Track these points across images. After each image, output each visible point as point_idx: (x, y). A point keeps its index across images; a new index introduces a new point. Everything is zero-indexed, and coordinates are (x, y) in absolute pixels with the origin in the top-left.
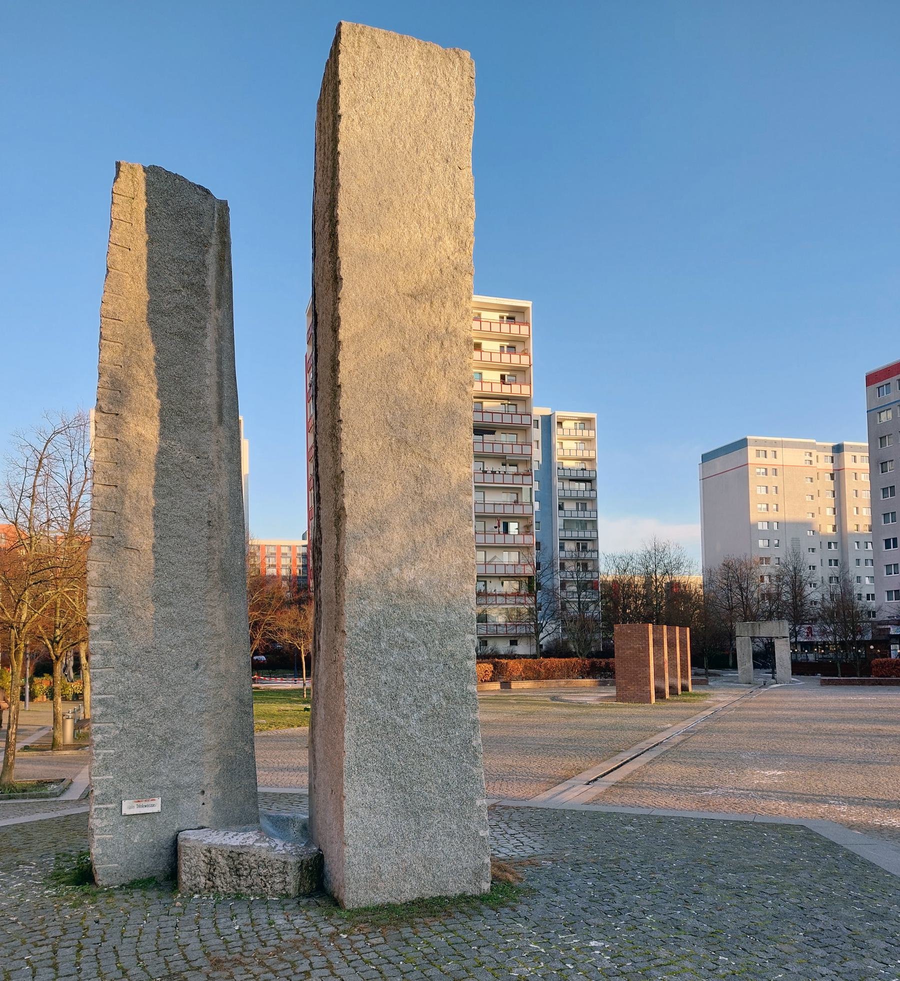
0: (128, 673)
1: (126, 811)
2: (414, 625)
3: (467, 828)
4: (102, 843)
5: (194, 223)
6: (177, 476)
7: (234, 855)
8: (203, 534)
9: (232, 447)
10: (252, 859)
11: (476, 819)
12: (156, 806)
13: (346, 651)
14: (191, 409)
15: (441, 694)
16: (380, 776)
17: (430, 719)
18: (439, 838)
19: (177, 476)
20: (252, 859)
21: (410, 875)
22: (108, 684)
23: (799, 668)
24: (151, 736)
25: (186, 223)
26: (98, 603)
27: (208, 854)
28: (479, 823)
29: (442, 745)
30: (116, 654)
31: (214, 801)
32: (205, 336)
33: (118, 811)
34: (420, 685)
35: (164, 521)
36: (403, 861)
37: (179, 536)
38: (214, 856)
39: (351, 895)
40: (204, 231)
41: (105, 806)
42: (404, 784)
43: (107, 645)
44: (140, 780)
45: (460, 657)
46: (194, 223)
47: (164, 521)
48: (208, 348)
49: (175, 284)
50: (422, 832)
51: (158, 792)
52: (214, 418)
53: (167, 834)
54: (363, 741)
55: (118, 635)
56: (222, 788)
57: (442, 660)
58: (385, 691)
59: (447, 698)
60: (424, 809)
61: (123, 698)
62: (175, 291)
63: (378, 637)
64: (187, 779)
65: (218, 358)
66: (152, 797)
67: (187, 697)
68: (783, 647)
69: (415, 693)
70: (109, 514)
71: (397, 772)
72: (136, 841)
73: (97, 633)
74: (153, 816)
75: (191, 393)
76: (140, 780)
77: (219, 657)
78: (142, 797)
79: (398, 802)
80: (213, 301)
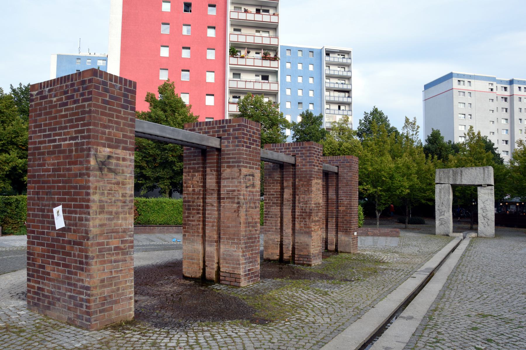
68: (486, 197)
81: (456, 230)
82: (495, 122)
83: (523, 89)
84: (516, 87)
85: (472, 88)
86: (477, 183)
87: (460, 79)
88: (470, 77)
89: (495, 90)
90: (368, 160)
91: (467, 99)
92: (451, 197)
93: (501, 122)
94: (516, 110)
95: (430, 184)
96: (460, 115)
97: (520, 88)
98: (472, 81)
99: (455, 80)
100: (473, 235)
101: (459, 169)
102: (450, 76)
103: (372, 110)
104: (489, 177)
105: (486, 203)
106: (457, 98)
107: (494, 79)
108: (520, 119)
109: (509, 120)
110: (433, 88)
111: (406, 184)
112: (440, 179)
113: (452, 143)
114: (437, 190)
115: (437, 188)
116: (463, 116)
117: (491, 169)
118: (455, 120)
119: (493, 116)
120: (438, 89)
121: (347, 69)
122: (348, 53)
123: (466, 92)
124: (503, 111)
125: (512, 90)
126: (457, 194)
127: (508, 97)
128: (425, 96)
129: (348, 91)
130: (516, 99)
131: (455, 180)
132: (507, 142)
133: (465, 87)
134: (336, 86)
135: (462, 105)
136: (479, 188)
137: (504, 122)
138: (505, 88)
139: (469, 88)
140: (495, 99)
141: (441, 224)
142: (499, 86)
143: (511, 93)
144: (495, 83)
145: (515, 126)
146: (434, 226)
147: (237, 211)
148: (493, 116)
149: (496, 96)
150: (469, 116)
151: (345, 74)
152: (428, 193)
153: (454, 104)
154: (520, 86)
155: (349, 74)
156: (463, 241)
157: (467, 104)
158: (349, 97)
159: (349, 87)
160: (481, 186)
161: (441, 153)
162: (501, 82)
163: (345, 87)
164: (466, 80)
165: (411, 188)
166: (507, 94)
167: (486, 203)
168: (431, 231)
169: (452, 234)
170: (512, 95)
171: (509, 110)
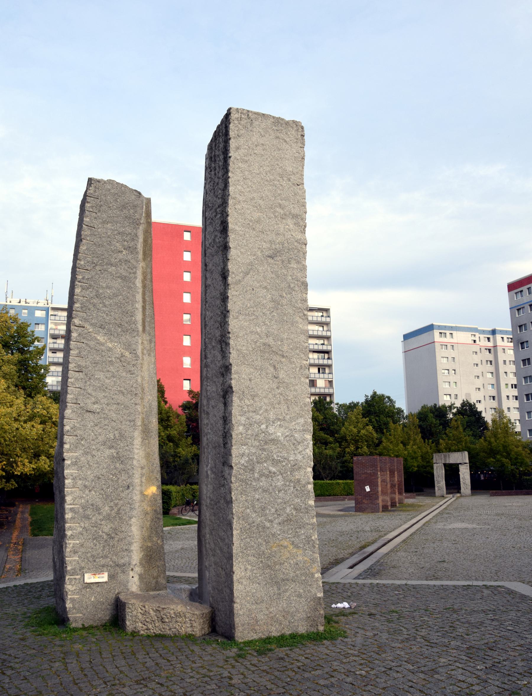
0: (87, 492)
1: (87, 580)
2: (275, 462)
3: (309, 591)
4: (73, 600)
5: (132, 211)
6: (117, 365)
7: (160, 609)
8: (133, 401)
9: (150, 346)
10: (172, 612)
11: (315, 586)
12: (104, 578)
13: (233, 479)
14: (127, 323)
15: (292, 506)
16: (255, 559)
17: (285, 523)
18: (292, 598)
19: (117, 365)
20: (172, 612)
21: (275, 622)
22: (76, 498)
23: (478, 486)
24: (101, 533)
25: (127, 212)
26: (70, 446)
27: (143, 608)
28: (317, 588)
29: (293, 539)
30: (80, 479)
31: (139, 575)
32: (136, 278)
33: (82, 580)
34: (280, 500)
35: (109, 393)
36: (271, 613)
37: (118, 404)
38: (147, 610)
39: (239, 634)
40: (137, 216)
41: (74, 577)
42: (270, 564)
43: (75, 473)
44: (95, 561)
45: (303, 482)
46: (132, 211)
47: (109, 393)
48: (138, 285)
49: (119, 246)
50: (282, 595)
51: (105, 569)
52: (140, 328)
53: (112, 596)
54: (245, 537)
55: (81, 467)
56: (144, 567)
57: (292, 484)
58: (257, 505)
59: (295, 509)
60: (283, 580)
61: (85, 508)
62: (119, 252)
63: (252, 470)
64: (123, 561)
65: (143, 291)
66: (102, 572)
67: (122, 508)
68: (464, 470)
69: (276, 506)
70: (77, 389)
71: (266, 557)
72: (92, 600)
73: (69, 465)
74: (103, 584)
75: (127, 313)
76: (95, 561)
77: (142, 482)
78: (97, 570)
79: (267, 575)
80: (141, 256)
81: (447, 493)
82: (481, 377)
83: (505, 339)
84: (498, 337)
85: (454, 340)
86: (458, 462)
87: (441, 331)
88: (452, 328)
89: (477, 342)
90: (391, 450)
91: (450, 353)
92: (444, 471)
93: (486, 376)
94: (501, 362)
95: (428, 462)
96: (443, 371)
97: (502, 338)
98: (454, 333)
99: (436, 333)
100: (458, 495)
101: (447, 454)
102: (430, 328)
103: (372, 393)
104: (465, 458)
105: (465, 473)
106: (440, 353)
107: (476, 330)
108: (506, 373)
109: (494, 374)
110: (413, 339)
111: (416, 464)
112: (436, 460)
113: (437, 406)
114: (435, 468)
115: (435, 466)
116: (447, 371)
117: (466, 453)
118: (438, 376)
119: (478, 371)
120: (419, 340)
121: (325, 328)
122: (327, 310)
123: (449, 345)
124: (487, 363)
125: (495, 341)
126: (447, 468)
127: (492, 348)
128: (405, 348)
129: (328, 352)
130: (499, 350)
131: (445, 460)
132: (494, 398)
133: (448, 339)
134: (316, 347)
135: (445, 359)
136: (460, 465)
137: (489, 376)
138: (489, 339)
139: (451, 340)
140: (478, 351)
141: (439, 489)
142: (482, 336)
143: (494, 344)
144: (477, 335)
145: (501, 380)
146: (435, 493)
147: (387, 485)
148: (478, 371)
149: (479, 348)
150: (453, 372)
151: (324, 334)
152: (428, 469)
153: (437, 359)
154: (503, 336)
155: (328, 334)
156: (451, 499)
157: (450, 359)
158: (329, 358)
159: (329, 348)
160: (461, 464)
161: (431, 429)
162: (483, 332)
163: (325, 348)
164: (448, 332)
165: (418, 466)
166: (490, 344)
167: (465, 473)
168: (433, 494)
169: (445, 496)
170: (495, 346)
171: (493, 363)
